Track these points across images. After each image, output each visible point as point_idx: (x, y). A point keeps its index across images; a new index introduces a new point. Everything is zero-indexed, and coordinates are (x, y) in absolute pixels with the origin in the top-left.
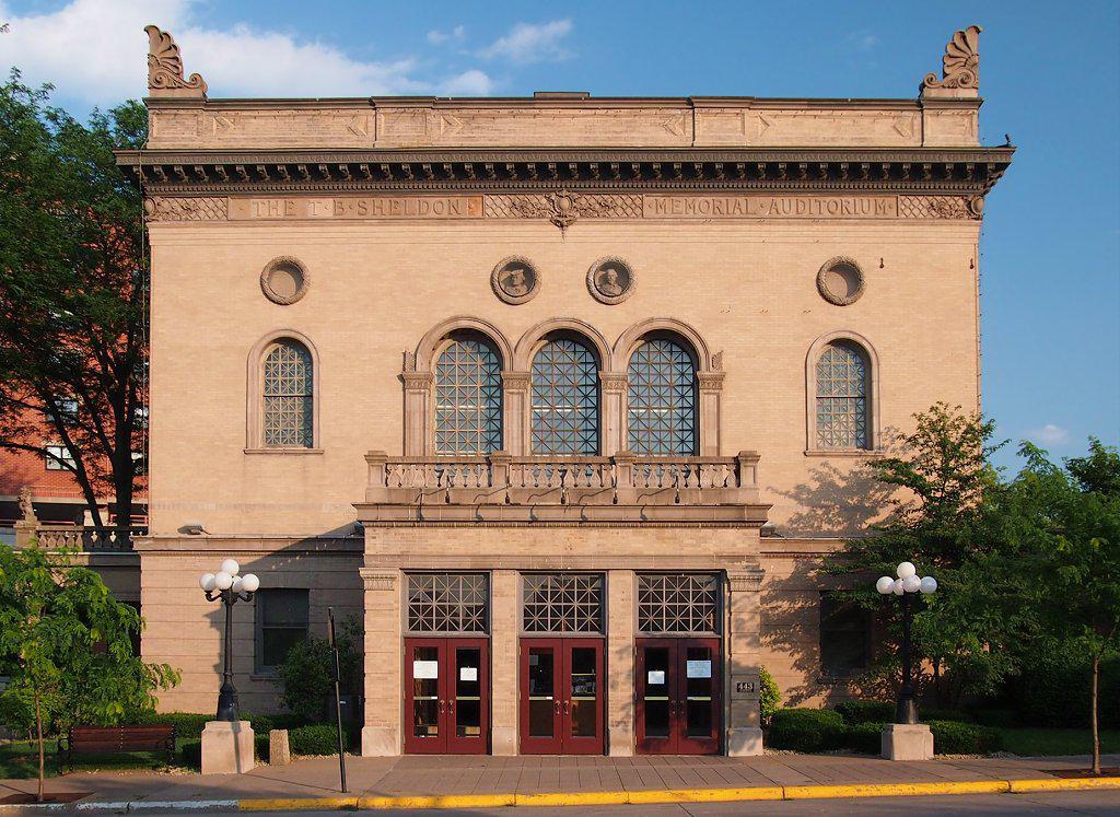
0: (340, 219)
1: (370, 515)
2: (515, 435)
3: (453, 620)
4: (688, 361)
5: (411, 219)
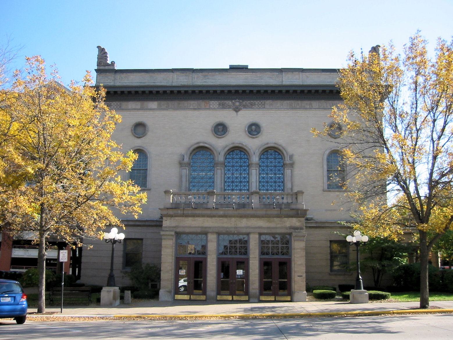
0: (160, 109)
1: (165, 212)
2: (219, 184)
3: (245, 251)
4: (281, 157)
5: (185, 109)
